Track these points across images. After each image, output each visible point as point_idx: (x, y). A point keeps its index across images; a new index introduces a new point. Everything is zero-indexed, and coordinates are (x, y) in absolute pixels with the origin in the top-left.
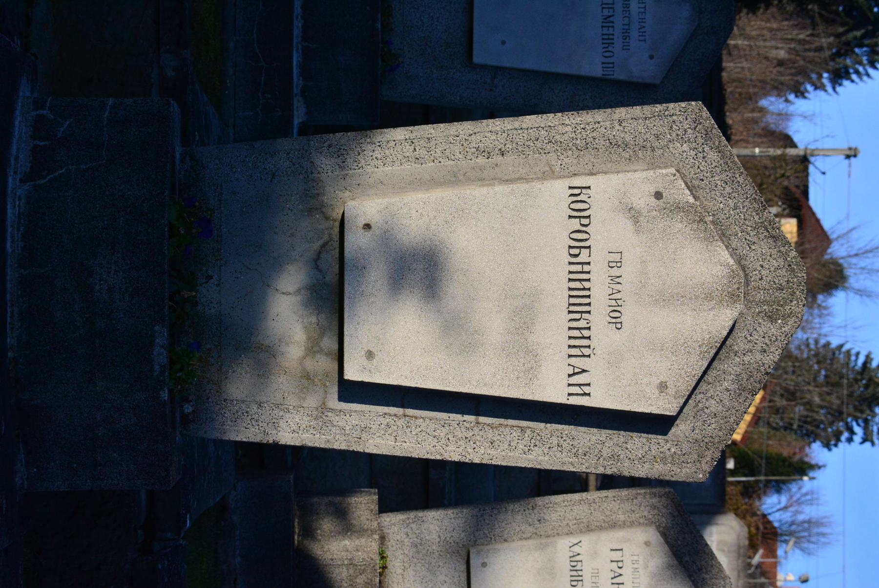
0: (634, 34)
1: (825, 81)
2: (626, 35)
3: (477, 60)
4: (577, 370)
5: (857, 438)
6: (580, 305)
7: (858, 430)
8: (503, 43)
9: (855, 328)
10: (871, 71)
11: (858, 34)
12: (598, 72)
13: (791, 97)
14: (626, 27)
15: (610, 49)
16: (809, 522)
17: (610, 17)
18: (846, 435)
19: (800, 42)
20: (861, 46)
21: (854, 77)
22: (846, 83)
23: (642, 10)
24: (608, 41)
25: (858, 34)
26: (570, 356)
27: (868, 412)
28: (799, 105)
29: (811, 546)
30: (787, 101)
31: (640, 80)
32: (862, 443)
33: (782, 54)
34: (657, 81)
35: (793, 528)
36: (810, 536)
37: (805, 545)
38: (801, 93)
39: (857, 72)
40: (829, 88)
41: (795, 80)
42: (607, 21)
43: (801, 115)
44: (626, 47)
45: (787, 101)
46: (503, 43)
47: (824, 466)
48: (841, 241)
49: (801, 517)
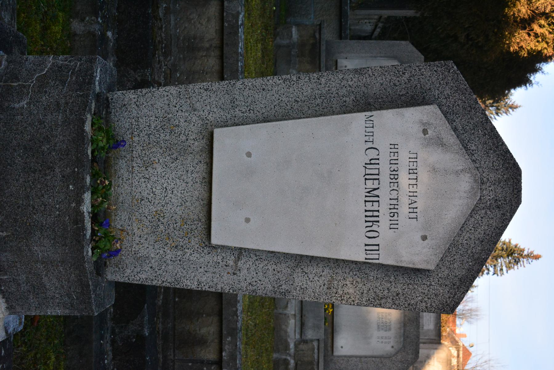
0: (404, 209)
2: (394, 213)
3: (215, 241)
4: (413, 202)
5: (491, 273)
6: (373, 216)
7: (491, 269)
8: (248, 220)
10: (496, 117)
12: (361, 257)
14: (395, 202)
15: (374, 228)
16: (471, 310)
17: (375, 189)
18: (486, 271)
20: (492, 106)
23: (414, 182)
24: (372, 218)
26: (378, 159)
27: (496, 262)
29: (472, 320)
31: (411, 266)
34: (432, 267)
35: (464, 312)
36: (471, 315)
37: (469, 320)
42: (372, 195)
44: (394, 226)
46: (248, 220)
47: (478, 286)
49: (467, 308)
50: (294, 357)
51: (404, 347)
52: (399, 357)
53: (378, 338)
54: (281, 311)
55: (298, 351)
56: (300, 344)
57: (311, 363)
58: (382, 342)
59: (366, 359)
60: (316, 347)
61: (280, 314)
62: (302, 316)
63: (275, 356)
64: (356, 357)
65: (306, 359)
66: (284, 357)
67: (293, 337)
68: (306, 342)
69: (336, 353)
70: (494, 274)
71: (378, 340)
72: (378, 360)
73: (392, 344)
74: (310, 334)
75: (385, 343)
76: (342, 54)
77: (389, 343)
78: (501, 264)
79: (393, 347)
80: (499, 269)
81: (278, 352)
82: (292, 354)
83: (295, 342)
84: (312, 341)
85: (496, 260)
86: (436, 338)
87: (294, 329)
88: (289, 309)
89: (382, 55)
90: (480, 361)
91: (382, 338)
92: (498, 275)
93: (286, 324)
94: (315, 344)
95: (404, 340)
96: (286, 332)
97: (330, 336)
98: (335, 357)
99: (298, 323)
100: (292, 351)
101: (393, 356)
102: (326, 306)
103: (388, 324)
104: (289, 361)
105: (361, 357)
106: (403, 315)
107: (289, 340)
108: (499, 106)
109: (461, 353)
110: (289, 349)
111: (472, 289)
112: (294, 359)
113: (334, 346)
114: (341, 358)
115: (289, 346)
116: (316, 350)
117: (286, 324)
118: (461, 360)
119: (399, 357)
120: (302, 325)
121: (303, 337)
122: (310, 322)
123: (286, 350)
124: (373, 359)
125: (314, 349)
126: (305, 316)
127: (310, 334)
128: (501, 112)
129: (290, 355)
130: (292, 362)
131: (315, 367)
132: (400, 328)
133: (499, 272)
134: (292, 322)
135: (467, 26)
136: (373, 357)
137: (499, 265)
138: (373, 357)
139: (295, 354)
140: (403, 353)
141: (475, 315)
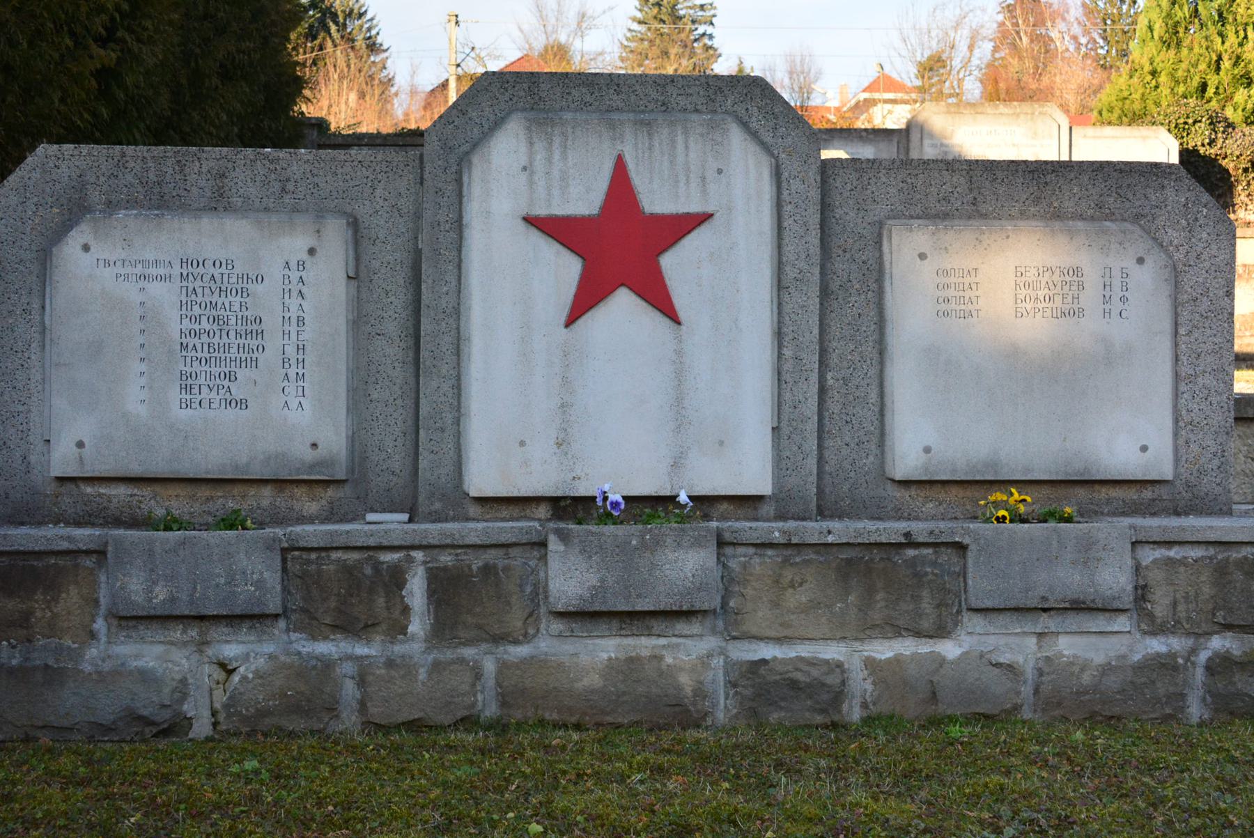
1: (378, 59)
5: (709, 30)
9: (615, 27)
10: (369, 16)
11: (333, 28)
13: (393, 90)
16: (791, 73)
19: (341, 78)
20: (345, 25)
21: (374, 32)
22: (379, 40)
25: (333, 28)
28: (402, 81)
29: (813, 71)
30: (396, 94)
32: (447, 80)
33: (353, 97)
35: (797, 89)
37: (812, 75)
38: (390, 81)
39: (369, 29)
40: (384, 55)
41: (379, 86)
43: (412, 77)
45: (396, 94)
48: (532, 40)
49: (787, 81)
50: (1198, 635)
51: (1137, 218)
52: (1174, 236)
53: (1106, 313)
54: (1027, 691)
55: (1178, 622)
56: (1151, 616)
57: (1221, 571)
58: (1124, 299)
59: (1183, 358)
60: (1159, 553)
61: (1036, 691)
62: (1045, 610)
63: (1195, 710)
64: (1177, 395)
65: (1207, 590)
66: (1200, 675)
67: (1126, 639)
68: (1142, 593)
69: (1166, 470)
70: (712, 24)
71: (1115, 313)
72: (1185, 314)
73: (1130, 264)
74: (1114, 578)
75: (1125, 287)
76: (33, 459)
77: (1125, 274)
78: (691, 8)
79: (1140, 261)
80: (700, 13)
81: (1182, 696)
82: (1190, 642)
83: (1145, 633)
84: (1138, 568)
85: (680, 18)
86: (895, 140)
87: (1093, 639)
88: (1021, 660)
89: (36, 305)
90: (904, 53)
91: (1106, 300)
92: (714, 16)
93: (1076, 669)
94: (1149, 555)
95: (1110, 217)
96: (1106, 669)
97: (1104, 493)
98: (1177, 475)
99: (1074, 621)
100: (1176, 644)
101: (1171, 257)
102: (1002, 513)
103: (1056, 278)
104: (1216, 654)
105: (1177, 376)
106: (1021, 223)
107: (1137, 657)
108: (344, 12)
109: (876, 96)
110: (1172, 655)
111: (747, 71)
112: (1209, 634)
113: (1140, 477)
114: (1182, 451)
115: (1158, 655)
116: (1173, 553)
117: (1076, 669)
118: (899, 96)
119: (1174, 236)
120: (1079, 607)
121: (1127, 601)
122: (1069, 579)
123: (1175, 668)
124: (1182, 331)
125: (1170, 562)
126: (1044, 599)
127: (1114, 578)
128: (356, 7)
129: (1194, 651)
130: (1218, 643)
131: (1235, 555)
132: (1071, 234)
133: (708, 13)
134: (1067, 646)
135: (69, 42)
136: (1176, 332)
137: (692, 12)
138: (1176, 332)
139: (1188, 634)
140: (1160, 221)
141: (802, 65)
